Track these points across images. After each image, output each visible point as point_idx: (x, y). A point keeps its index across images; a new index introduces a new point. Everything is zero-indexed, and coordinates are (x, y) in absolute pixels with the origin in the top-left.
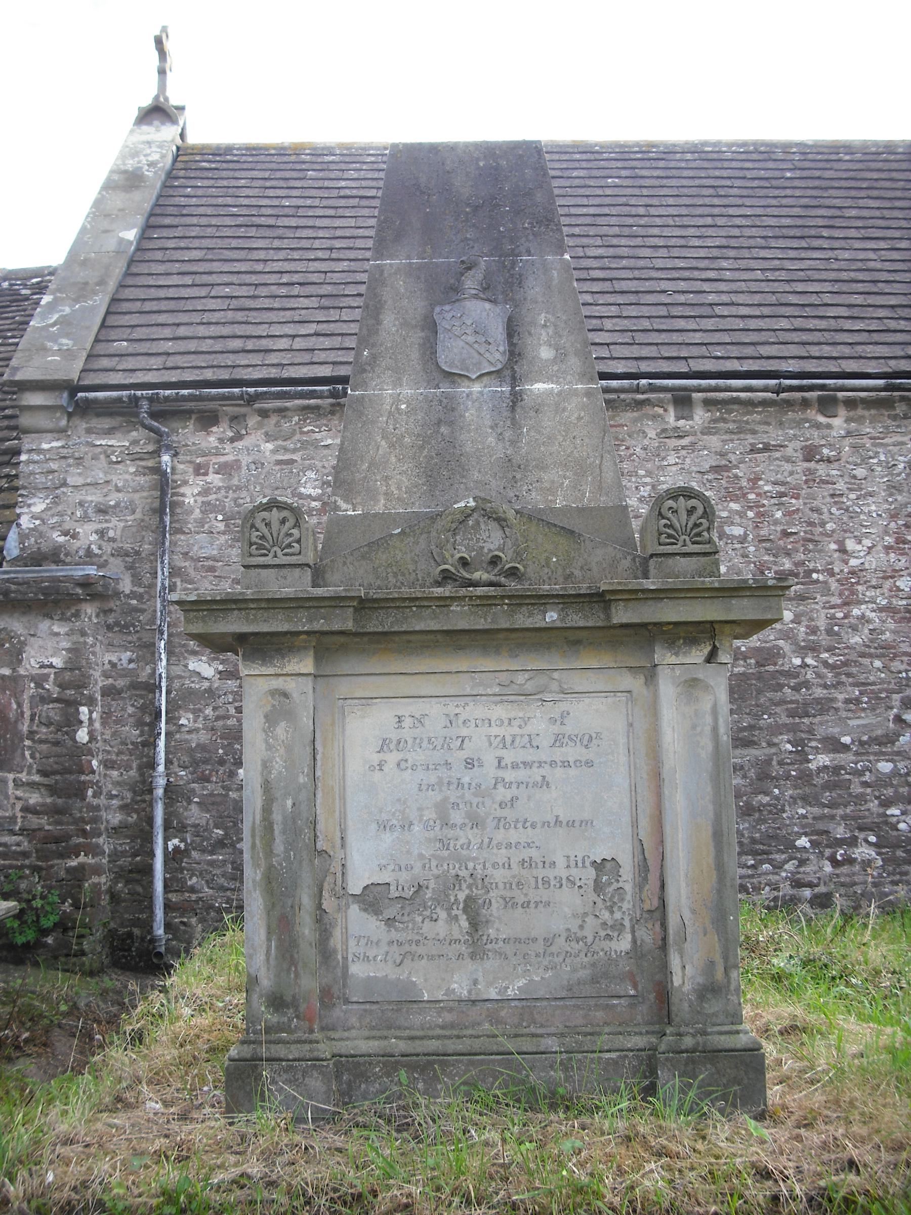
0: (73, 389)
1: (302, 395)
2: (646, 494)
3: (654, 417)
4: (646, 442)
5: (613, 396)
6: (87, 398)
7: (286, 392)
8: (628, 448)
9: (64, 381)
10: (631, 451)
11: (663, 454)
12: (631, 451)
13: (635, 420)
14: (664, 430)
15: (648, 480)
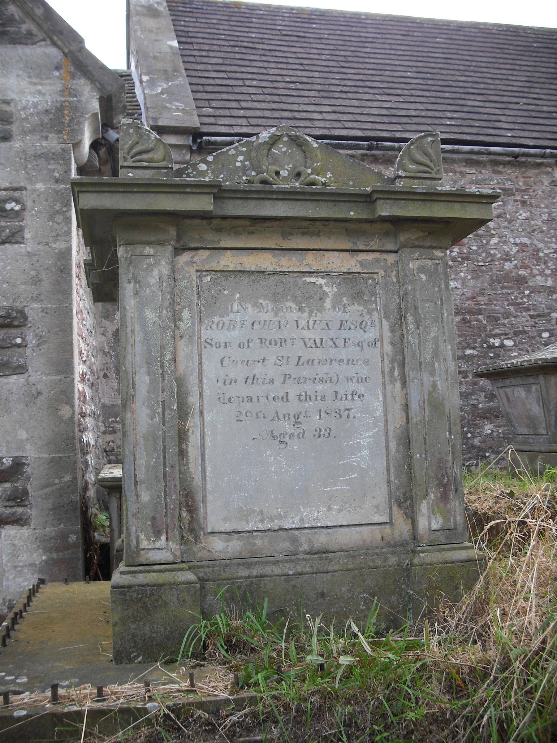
0: (196, 134)
1: (350, 147)
2: (546, 219)
3: (548, 173)
4: (544, 188)
5: (447, 155)
6: (209, 140)
7: (341, 144)
8: (534, 191)
9: (193, 128)
10: (536, 193)
11: (553, 195)
12: (536, 193)
13: (537, 175)
14: (553, 181)
15: (546, 210)
